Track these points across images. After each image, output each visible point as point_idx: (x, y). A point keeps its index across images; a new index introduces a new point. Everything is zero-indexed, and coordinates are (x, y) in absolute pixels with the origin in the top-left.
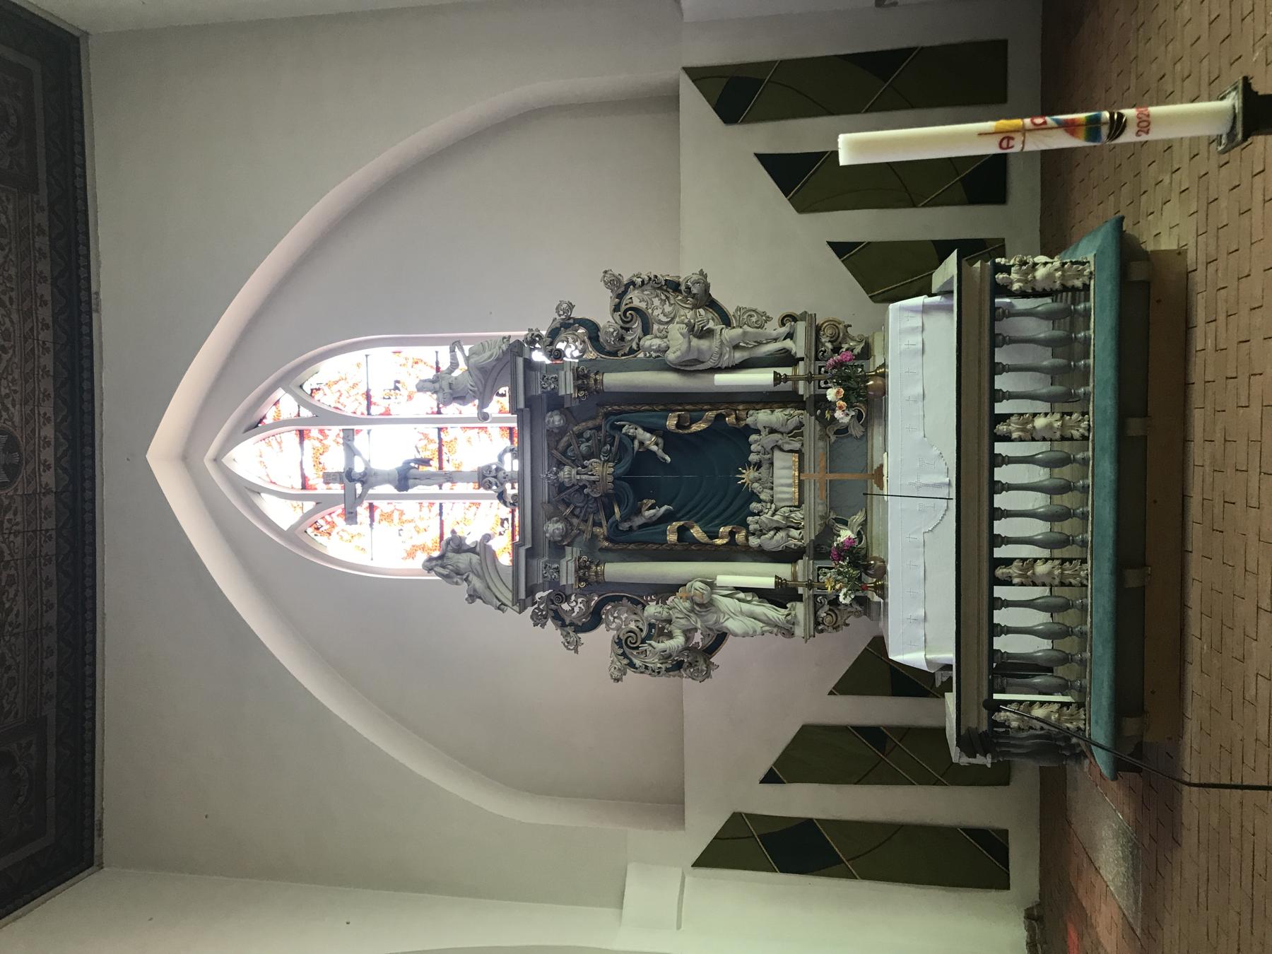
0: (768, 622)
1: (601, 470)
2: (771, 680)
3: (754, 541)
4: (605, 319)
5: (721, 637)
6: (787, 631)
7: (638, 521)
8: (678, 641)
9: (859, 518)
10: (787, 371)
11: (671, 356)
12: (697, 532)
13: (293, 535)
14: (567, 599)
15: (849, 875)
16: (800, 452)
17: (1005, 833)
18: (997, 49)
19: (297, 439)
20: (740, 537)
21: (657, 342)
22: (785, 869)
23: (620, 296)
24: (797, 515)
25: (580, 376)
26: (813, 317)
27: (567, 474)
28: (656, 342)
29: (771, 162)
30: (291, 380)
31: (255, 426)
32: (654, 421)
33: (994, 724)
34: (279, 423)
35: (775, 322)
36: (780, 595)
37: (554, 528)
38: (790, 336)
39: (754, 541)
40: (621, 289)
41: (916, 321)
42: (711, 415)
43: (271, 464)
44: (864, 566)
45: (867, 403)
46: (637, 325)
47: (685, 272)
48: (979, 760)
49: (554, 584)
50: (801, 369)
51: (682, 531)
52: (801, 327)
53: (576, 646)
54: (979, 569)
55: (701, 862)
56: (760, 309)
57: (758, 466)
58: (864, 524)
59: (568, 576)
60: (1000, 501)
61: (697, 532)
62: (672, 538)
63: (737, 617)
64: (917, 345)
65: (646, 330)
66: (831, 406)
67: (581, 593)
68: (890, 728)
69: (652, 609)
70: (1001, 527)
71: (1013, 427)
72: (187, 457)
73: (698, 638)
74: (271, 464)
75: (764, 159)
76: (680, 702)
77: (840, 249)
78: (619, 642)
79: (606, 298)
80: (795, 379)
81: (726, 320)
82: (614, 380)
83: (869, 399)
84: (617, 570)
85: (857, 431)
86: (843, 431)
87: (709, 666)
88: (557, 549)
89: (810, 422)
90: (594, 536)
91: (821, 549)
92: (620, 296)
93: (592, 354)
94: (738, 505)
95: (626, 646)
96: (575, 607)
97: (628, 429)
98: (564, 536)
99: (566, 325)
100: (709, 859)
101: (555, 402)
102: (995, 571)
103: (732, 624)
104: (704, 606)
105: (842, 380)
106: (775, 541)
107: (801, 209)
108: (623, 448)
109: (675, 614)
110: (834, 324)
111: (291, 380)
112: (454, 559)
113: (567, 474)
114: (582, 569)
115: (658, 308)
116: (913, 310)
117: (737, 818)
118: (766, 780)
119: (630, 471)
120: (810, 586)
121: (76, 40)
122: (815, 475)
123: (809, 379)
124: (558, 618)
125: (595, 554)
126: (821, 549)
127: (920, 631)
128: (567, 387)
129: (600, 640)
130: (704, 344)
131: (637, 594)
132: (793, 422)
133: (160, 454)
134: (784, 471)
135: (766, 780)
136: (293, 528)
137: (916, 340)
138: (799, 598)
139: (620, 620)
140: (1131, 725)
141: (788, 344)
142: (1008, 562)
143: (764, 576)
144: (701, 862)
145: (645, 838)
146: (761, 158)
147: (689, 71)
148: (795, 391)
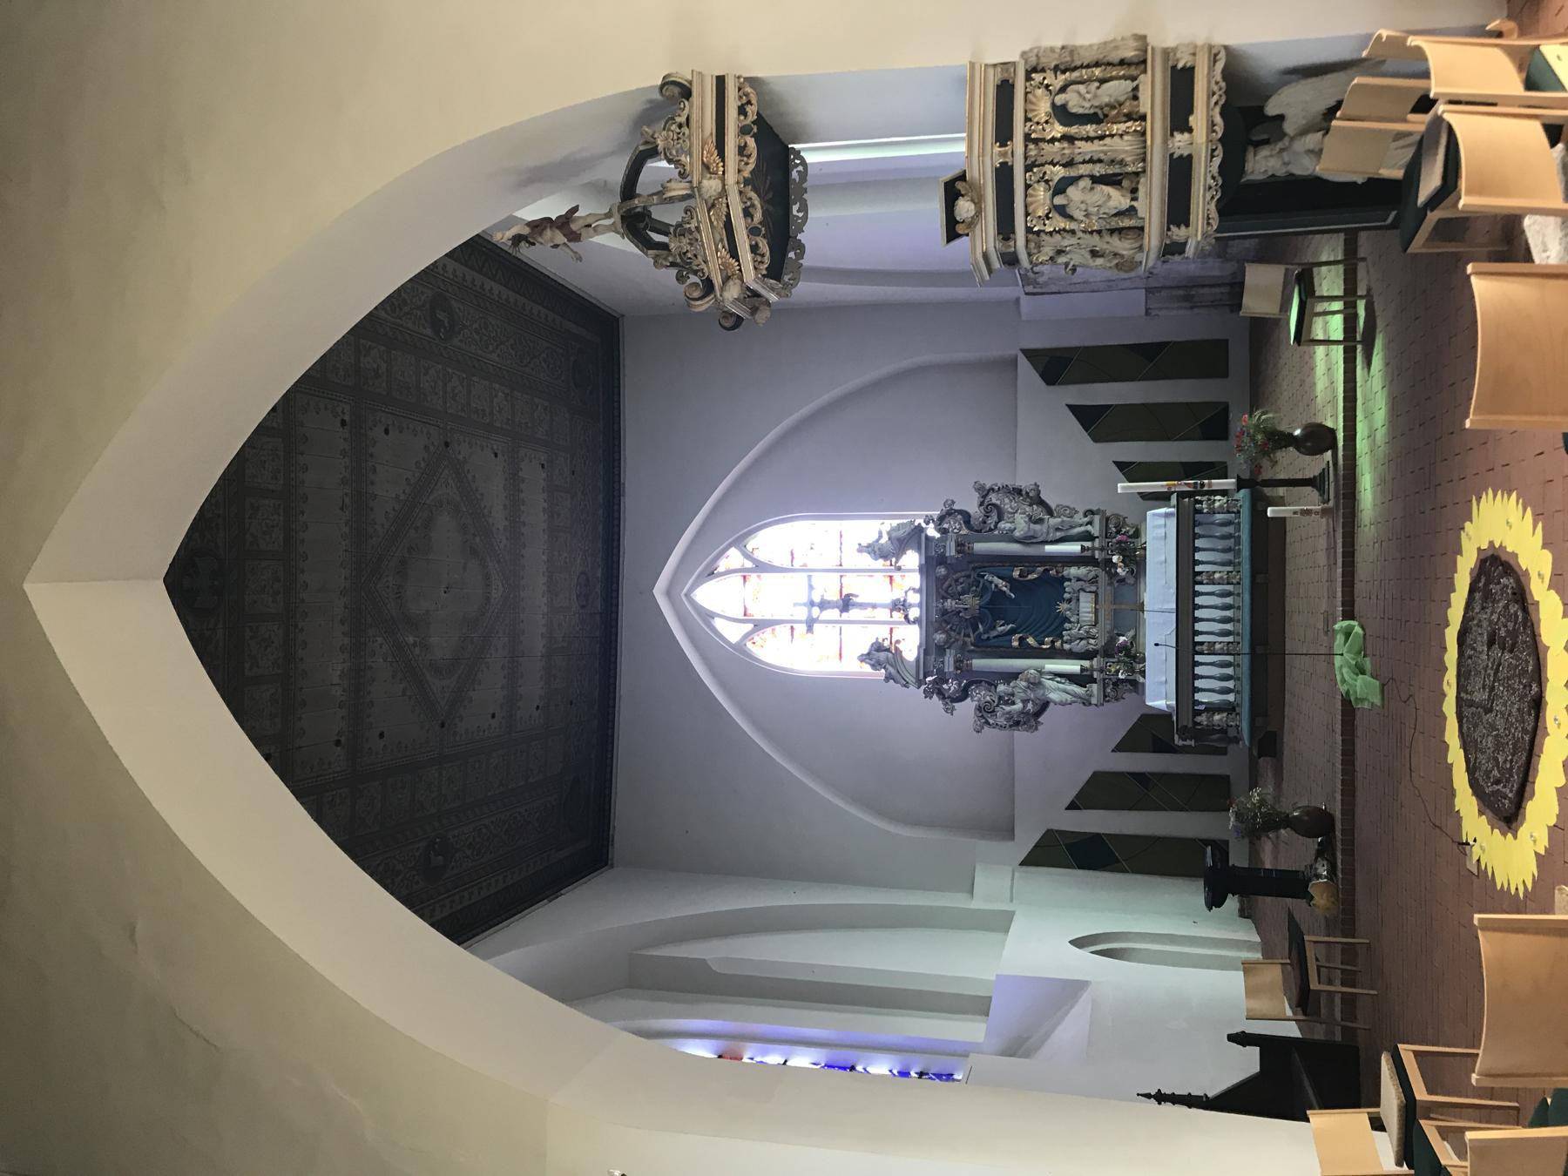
0: (1075, 695)
1: (971, 601)
2: (1073, 737)
3: (1067, 647)
4: (973, 508)
5: (1044, 705)
6: (1086, 702)
7: (994, 633)
8: (1019, 706)
9: (1131, 633)
10: (1088, 544)
11: (1017, 534)
12: (1031, 641)
13: (740, 647)
14: (946, 682)
15: (1124, 871)
16: (1096, 593)
17: (1227, 842)
18: (1221, 346)
19: (767, 577)
20: (1058, 644)
21: (1008, 526)
22: (1080, 867)
23: (984, 497)
24: (1094, 631)
25: (960, 546)
26: (1104, 512)
27: (949, 604)
28: (1008, 526)
29: (1076, 410)
30: (740, 542)
31: (711, 574)
33: (1196, 723)
34: (729, 572)
35: (1081, 514)
36: (1080, 679)
37: (939, 637)
38: (1090, 523)
39: (1067, 647)
40: (984, 492)
41: (1162, 521)
42: (1041, 569)
43: (708, 595)
44: (1133, 657)
45: (1137, 564)
47: (1024, 482)
48: (1188, 743)
49: (940, 671)
50: (1097, 543)
51: (1021, 640)
52: (1097, 518)
53: (950, 711)
54: (1187, 648)
55: (1023, 864)
57: (1069, 601)
58: (1134, 637)
59: (949, 667)
60: (1198, 613)
61: (1031, 641)
62: (1015, 644)
63: (1056, 692)
64: (1159, 532)
65: (1000, 519)
66: (1115, 566)
67: (956, 678)
68: (1153, 774)
69: (1001, 688)
70: (1198, 626)
71: (1204, 578)
72: (668, 593)
73: (1030, 706)
74: (708, 595)
75: (1072, 408)
76: (1012, 753)
78: (979, 709)
80: (1093, 549)
81: (1050, 512)
82: (980, 547)
83: (1136, 563)
84: (978, 663)
85: (1131, 581)
86: (1122, 580)
87: (1038, 723)
88: (941, 650)
90: (965, 643)
91: (1108, 651)
92: (984, 497)
93: (965, 531)
94: (1057, 625)
95: (984, 711)
96: (951, 687)
97: (988, 577)
98: (946, 642)
99: (950, 513)
100: (1031, 860)
101: (942, 560)
102: (1196, 648)
103: (1053, 696)
104: (1035, 684)
105: (1121, 551)
106: (1079, 646)
107: (1096, 440)
108: (985, 588)
109: (1016, 690)
110: (1117, 516)
111: (740, 542)
112: (882, 655)
113: (949, 604)
114: (958, 664)
115: (1008, 504)
116: (1159, 515)
117: (1049, 834)
118: (1068, 808)
119: (991, 602)
120: (1101, 671)
121: (617, 320)
122: (1105, 608)
123: (1102, 549)
124: (941, 694)
126: (1108, 651)
127: (1160, 695)
128: (951, 551)
129: (967, 708)
130: (1037, 527)
131: (990, 680)
132: (1092, 574)
134: (1086, 605)
135: (1068, 808)
136: (738, 643)
137: (1161, 532)
138: (1094, 681)
139: (980, 695)
141: (1089, 528)
142: (1202, 643)
143: (1073, 667)
144: (1023, 864)
145: (984, 846)
146: (1069, 406)
147: (1024, 352)
148: (1093, 556)
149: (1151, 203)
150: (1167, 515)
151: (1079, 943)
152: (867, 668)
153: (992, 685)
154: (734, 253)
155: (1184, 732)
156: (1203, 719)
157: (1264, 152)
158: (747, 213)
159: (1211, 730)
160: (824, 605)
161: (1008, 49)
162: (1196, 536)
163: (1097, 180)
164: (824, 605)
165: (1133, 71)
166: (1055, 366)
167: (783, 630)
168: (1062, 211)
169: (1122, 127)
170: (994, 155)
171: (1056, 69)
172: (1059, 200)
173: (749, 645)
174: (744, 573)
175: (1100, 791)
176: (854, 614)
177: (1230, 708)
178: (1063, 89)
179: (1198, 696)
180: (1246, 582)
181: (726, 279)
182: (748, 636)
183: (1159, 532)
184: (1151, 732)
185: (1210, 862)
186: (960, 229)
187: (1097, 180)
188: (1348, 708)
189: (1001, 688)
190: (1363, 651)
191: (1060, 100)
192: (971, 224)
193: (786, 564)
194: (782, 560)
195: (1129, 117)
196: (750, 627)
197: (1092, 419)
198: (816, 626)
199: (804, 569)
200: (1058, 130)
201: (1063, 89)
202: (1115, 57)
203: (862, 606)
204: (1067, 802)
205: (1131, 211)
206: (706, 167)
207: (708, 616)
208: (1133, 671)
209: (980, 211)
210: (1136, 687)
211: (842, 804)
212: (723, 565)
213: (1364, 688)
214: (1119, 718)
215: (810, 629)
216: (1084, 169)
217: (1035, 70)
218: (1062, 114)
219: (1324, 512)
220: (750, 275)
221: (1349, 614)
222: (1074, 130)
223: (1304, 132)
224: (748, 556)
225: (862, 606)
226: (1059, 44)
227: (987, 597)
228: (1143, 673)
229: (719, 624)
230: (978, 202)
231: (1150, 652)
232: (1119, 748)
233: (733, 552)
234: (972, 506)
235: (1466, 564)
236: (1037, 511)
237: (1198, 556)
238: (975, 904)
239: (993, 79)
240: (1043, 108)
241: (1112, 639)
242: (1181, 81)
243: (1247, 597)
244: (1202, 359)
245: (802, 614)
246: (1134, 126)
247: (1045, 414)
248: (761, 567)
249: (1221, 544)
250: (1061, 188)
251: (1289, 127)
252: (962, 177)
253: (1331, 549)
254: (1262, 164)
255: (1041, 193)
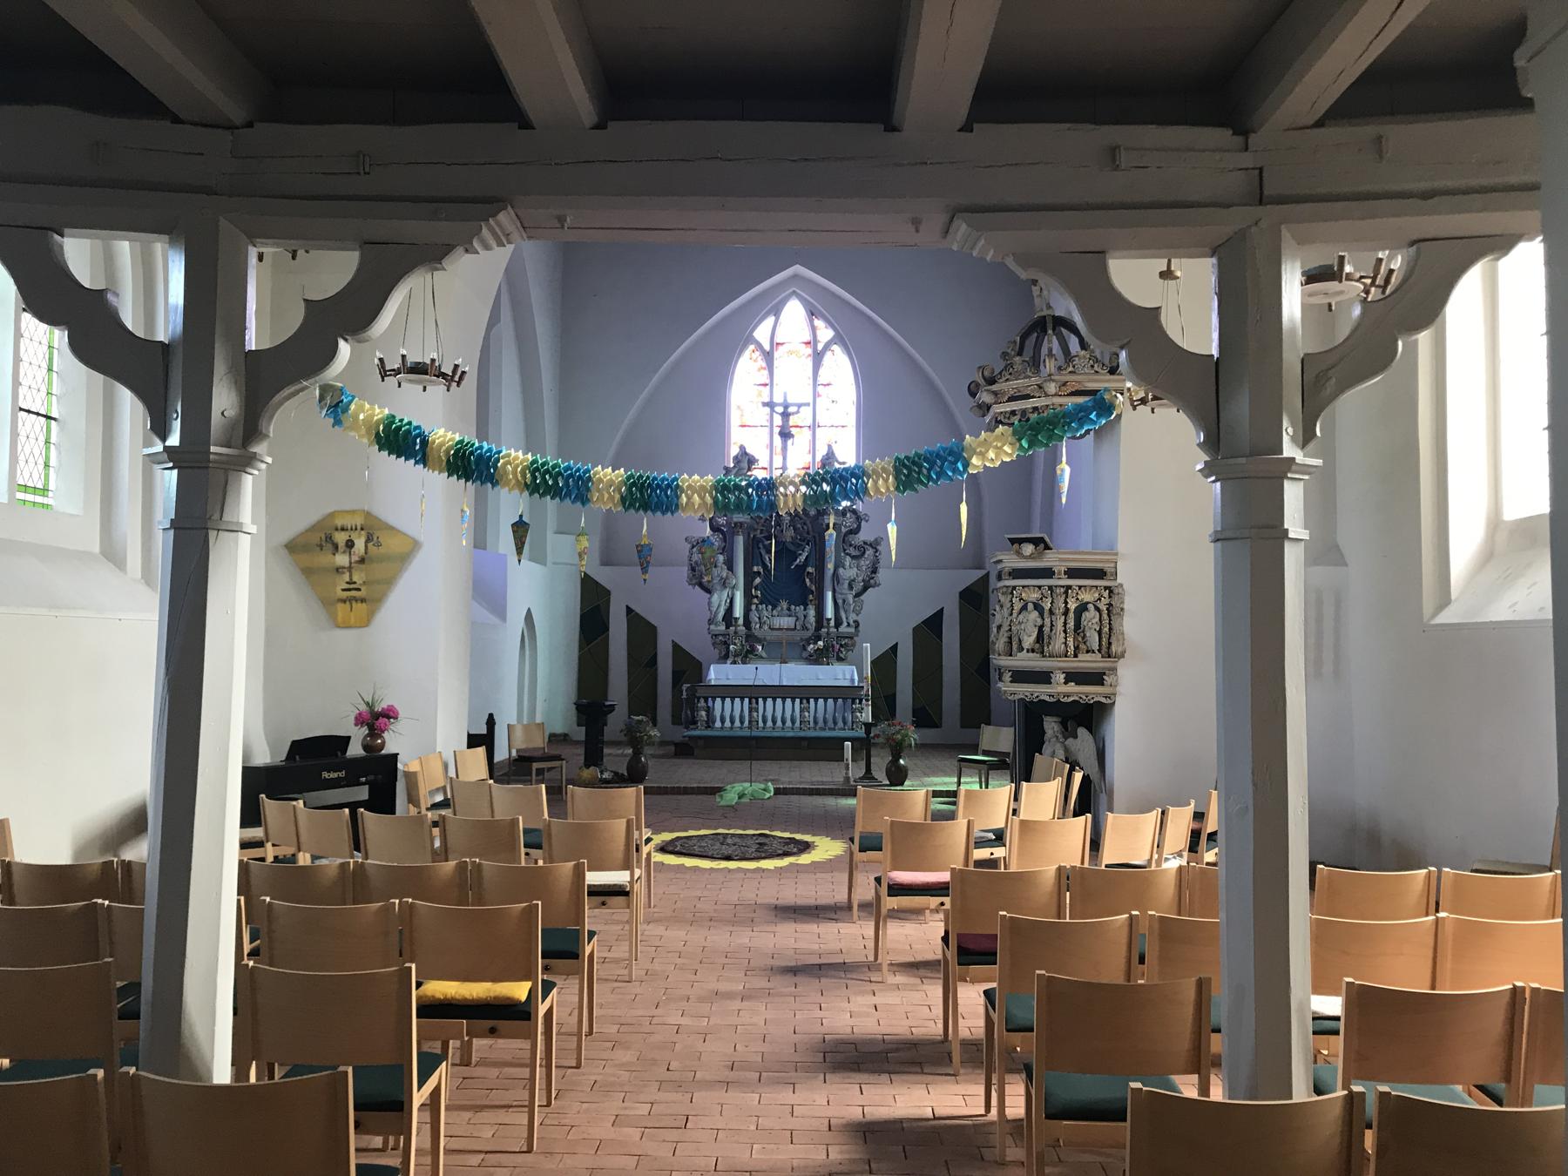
0: (716, 613)
2: (683, 612)
5: (708, 591)
6: (711, 622)
10: (832, 623)
11: (841, 570)
12: (758, 580)
13: (750, 339)
15: (581, 648)
19: (809, 363)
29: (939, 614)
31: (812, 313)
32: (812, 561)
34: (814, 329)
36: (729, 617)
43: (794, 311)
44: (747, 655)
46: (857, 553)
47: (882, 575)
54: (754, 693)
56: (1131, 626)
61: (758, 580)
63: (719, 599)
64: (840, 674)
65: (853, 557)
69: (721, 558)
70: (770, 701)
72: (795, 276)
74: (794, 311)
75: (940, 613)
77: (894, 648)
79: (871, 539)
81: (858, 595)
83: (817, 658)
84: (740, 541)
85: (805, 654)
86: (804, 648)
89: (809, 633)
91: (751, 638)
94: (771, 600)
96: (722, 521)
102: (754, 699)
103: (715, 597)
106: (754, 616)
108: (799, 546)
112: (746, 460)
115: (865, 563)
117: (608, 593)
125: (747, 530)
126: (751, 638)
127: (716, 674)
131: (727, 549)
133: (798, 269)
134: (787, 622)
139: (716, 541)
140: (701, 743)
143: (738, 612)
149: (1025, 661)
150: (852, 680)
151: (529, 617)
152: (734, 451)
153: (723, 551)
154: (1010, 400)
155: (692, 691)
156: (702, 703)
157: (1057, 727)
158: (1035, 409)
159: (694, 709)
160: (786, 415)
161: (1126, 576)
162: (836, 700)
163: (1041, 628)
164: (786, 415)
165: (1104, 649)
166: (975, 600)
167: (764, 377)
168: (1024, 608)
169: (1071, 644)
170: (1060, 568)
171: (1110, 605)
172: (1030, 606)
173: (752, 347)
174: (812, 343)
175: (642, 632)
176: (778, 440)
177: (709, 723)
178: (1097, 609)
179: (718, 700)
180: (802, 734)
181: (995, 393)
182: (759, 346)
183: (840, 674)
184: (688, 668)
185: (1400, 343)
186: (1016, 546)
187: (1041, 628)
188: (715, 791)
189: (721, 558)
190: (754, 798)
191: (1091, 607)
192: (1019, 553)
193: (821, 380)
194: (824, 376)
195: (1077, 648)
196: (767, 347)
197: (933, 624)
198: (768, 410)
199: (815, 395)
200: (1072, 606)
201: (1097, 609)
202: (1113, 640)
203: (784, 449)
204: (633, 607)
205: (1021, 649)
206: (1065, 384)
207: (777, 311)
208: (736, 656)
209: (1027, 557)
210: (724, 658)
211: (624, 426)
212: (819, 323)
213: (731, 796)
214: (699, 646)
215: (765, 404)
216: (1047, 621)
217: (1111, 592)
218: (1083, 608)
219: (847, 779)
220: (997, 409)
221: (778, 792)
222: (1071, 615)
223: (1066, 750)
224: (827, 346)
225: (784, 449)
226: (1126, 606)
227: (792, 548)
228: (734, 662)
229: (770, 320)
230: (1031, 557)
231: (750, 667)
232: (676, 646)
233: (830, 334)
234: (865, 535)
235: (807, 838)
236: (859, 586)
237: (821, 701)
238: (550, 535)
239: (1107, 567)
240: (1086, 597)
241: (759, 641)
242: (1096, 678)
243: (791, 734)
244: (978, 709)
245: (778, 399)
246: (1071, 650)
247: (939, 591)
248: (818, 358)
249: (830, 717)
250: (1037, 607)
251: (1070, 741)
252: (1047, 547)
253: (823, 783)
254: (1051, 726)
255: (1034, 596)
